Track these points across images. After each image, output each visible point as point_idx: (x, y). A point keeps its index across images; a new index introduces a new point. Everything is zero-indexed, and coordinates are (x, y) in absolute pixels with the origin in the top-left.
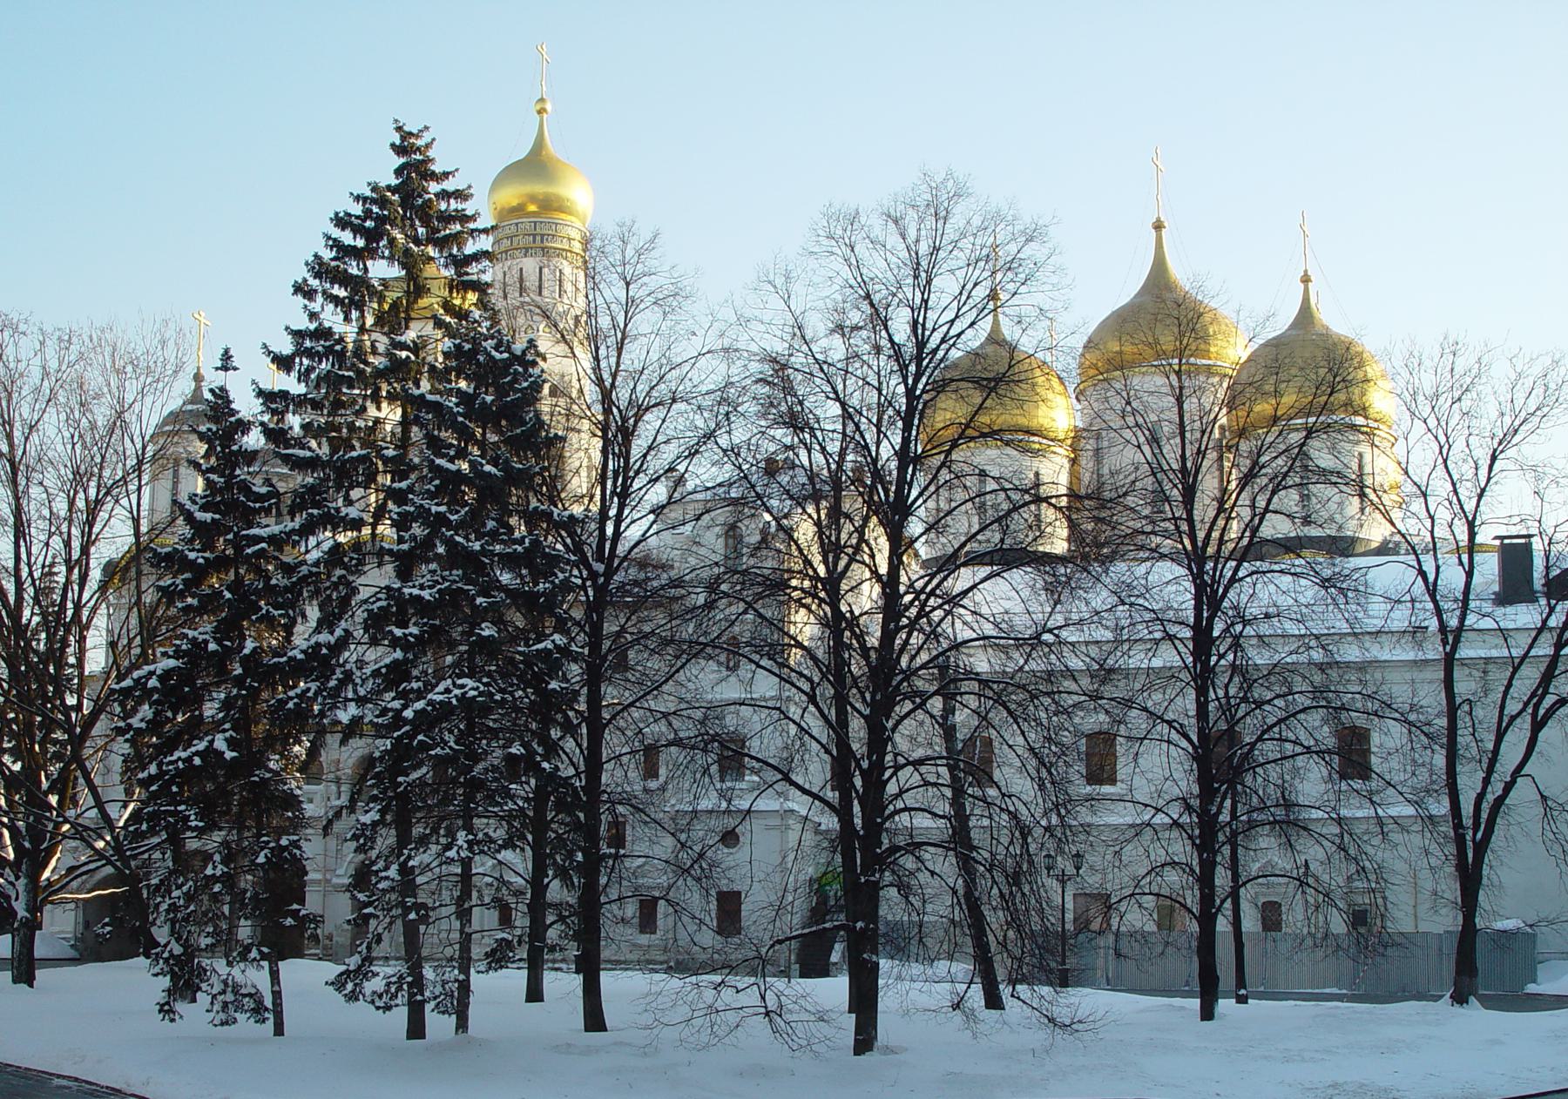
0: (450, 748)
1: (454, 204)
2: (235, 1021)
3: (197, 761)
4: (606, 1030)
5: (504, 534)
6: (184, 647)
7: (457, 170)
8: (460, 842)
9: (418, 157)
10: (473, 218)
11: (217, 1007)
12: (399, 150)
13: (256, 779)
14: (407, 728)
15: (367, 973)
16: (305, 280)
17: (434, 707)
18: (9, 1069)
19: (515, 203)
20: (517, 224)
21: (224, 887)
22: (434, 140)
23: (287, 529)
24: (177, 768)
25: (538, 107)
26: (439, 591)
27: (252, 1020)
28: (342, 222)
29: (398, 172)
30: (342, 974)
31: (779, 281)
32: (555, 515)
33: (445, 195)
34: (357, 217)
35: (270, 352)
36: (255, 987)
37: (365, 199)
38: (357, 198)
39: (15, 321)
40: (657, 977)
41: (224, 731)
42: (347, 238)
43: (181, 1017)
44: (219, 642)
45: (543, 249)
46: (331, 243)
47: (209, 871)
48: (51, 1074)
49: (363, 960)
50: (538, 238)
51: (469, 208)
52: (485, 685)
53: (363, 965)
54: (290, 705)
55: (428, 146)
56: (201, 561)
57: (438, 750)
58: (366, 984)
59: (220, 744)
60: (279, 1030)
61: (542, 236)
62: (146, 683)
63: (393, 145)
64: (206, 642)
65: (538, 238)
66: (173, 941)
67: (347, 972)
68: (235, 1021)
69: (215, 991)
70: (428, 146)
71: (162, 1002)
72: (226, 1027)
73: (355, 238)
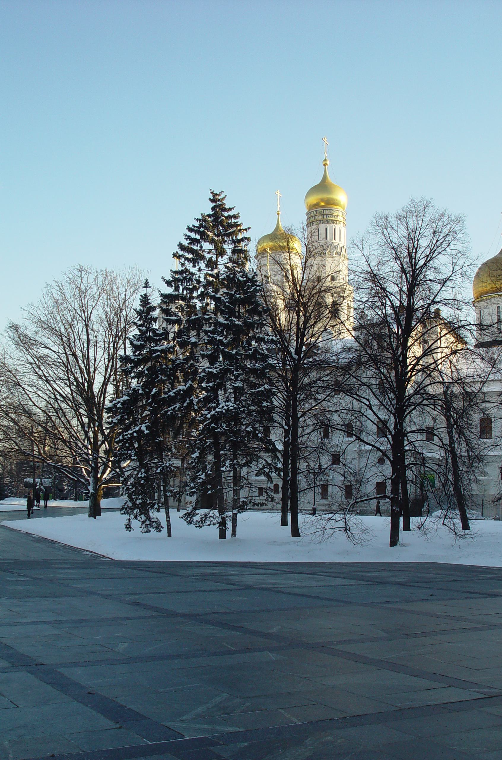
0: (224, 429)
1: (233, 220)
2: (150, 531)
3: (135, 434)
4: (299, 536)
5: (247, 347)
6: (130, 392)
7: (235, 207)
8: (227, 465)
9: (220, 203)
10: (240, 225)
11: (143, 526)
12: (212, 201)
13: (158, 441)
14: (209, 421)
15: (194, 513)
16: (177, 252)
17: (218, 413)
18: (72, 548)
19: (315, 203)
20: (316, 211)
21: (145, 481)
22: (226, 196)
23: (169, 347)
24: (128, 437)
25: (324, 163)
26: (220, 370)
27: (156, 531)
28: (190, 229)
29: (213, 209)
30: (185, 514)
31: (359, 244)
32: (266, 339)
33: (230, 217)
34: (197, 227)
35: (165, 280)
36: (157, 518)
37: (200, 220)
38: (197, 220)
39: (86, 268)
40: (307, 516)
41: (146, 423)
42: (193, 235)
43: (133, 530)
44: (143, 390)
45: (327, 220)
46: (187, 237)
47: (139, 476)
48: (84, 550)
49: (193, 509)
50: (325, 216)
51: (239, 221)
52: (236, 405)
53: (193, 511)
54: (169, 413)
55: (223, 199)
56: (136, 360)
57: (219, 430)
58: (194, 518)
59: (143, 428)
60: (169, 535)
61: (327, 215)
62: (117, 406)
63: (210, 199)
64: (139, 390)
65: (325, 216)
66: (129, 501)
67: (188, 513)
68: (150, 531)
69: (142, 520)
70: (223, 199)
71: (126, 524)
72: (147, 534)
73: (196, 235)
